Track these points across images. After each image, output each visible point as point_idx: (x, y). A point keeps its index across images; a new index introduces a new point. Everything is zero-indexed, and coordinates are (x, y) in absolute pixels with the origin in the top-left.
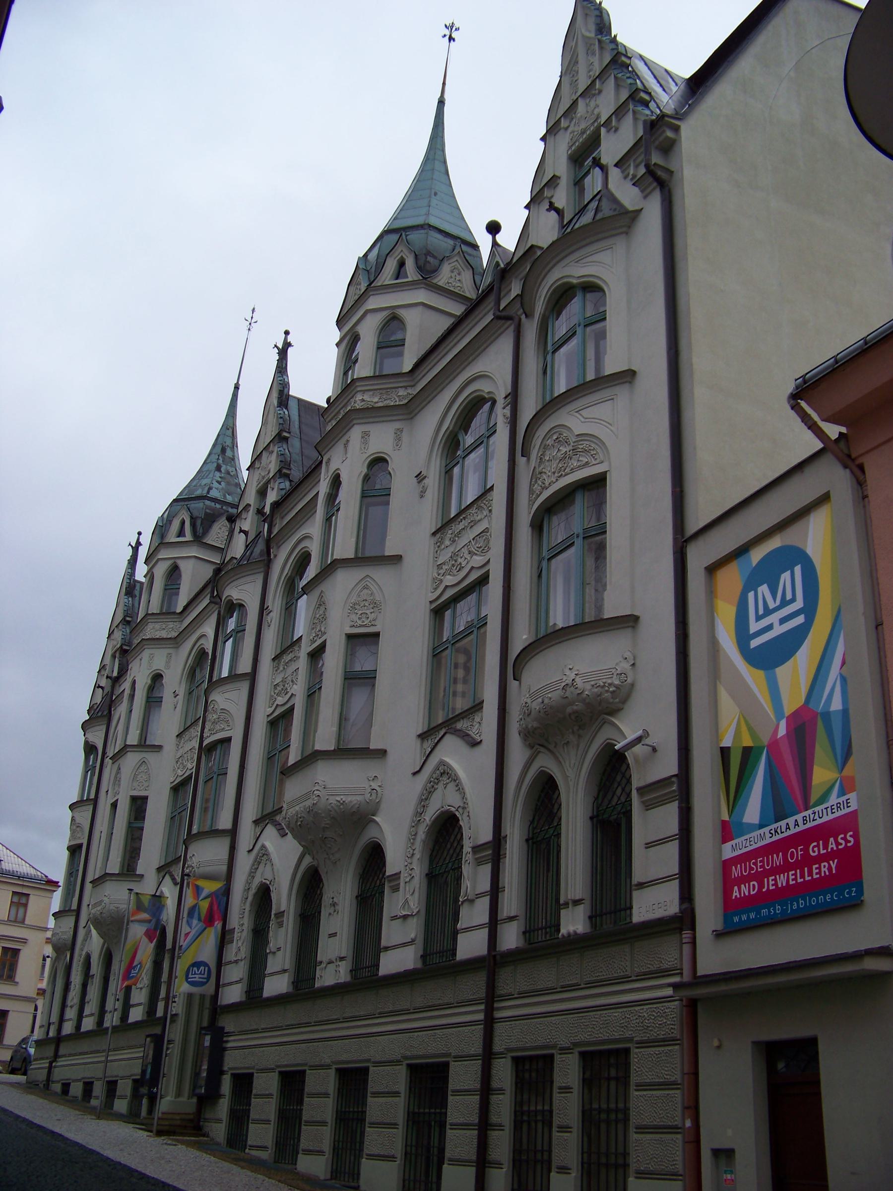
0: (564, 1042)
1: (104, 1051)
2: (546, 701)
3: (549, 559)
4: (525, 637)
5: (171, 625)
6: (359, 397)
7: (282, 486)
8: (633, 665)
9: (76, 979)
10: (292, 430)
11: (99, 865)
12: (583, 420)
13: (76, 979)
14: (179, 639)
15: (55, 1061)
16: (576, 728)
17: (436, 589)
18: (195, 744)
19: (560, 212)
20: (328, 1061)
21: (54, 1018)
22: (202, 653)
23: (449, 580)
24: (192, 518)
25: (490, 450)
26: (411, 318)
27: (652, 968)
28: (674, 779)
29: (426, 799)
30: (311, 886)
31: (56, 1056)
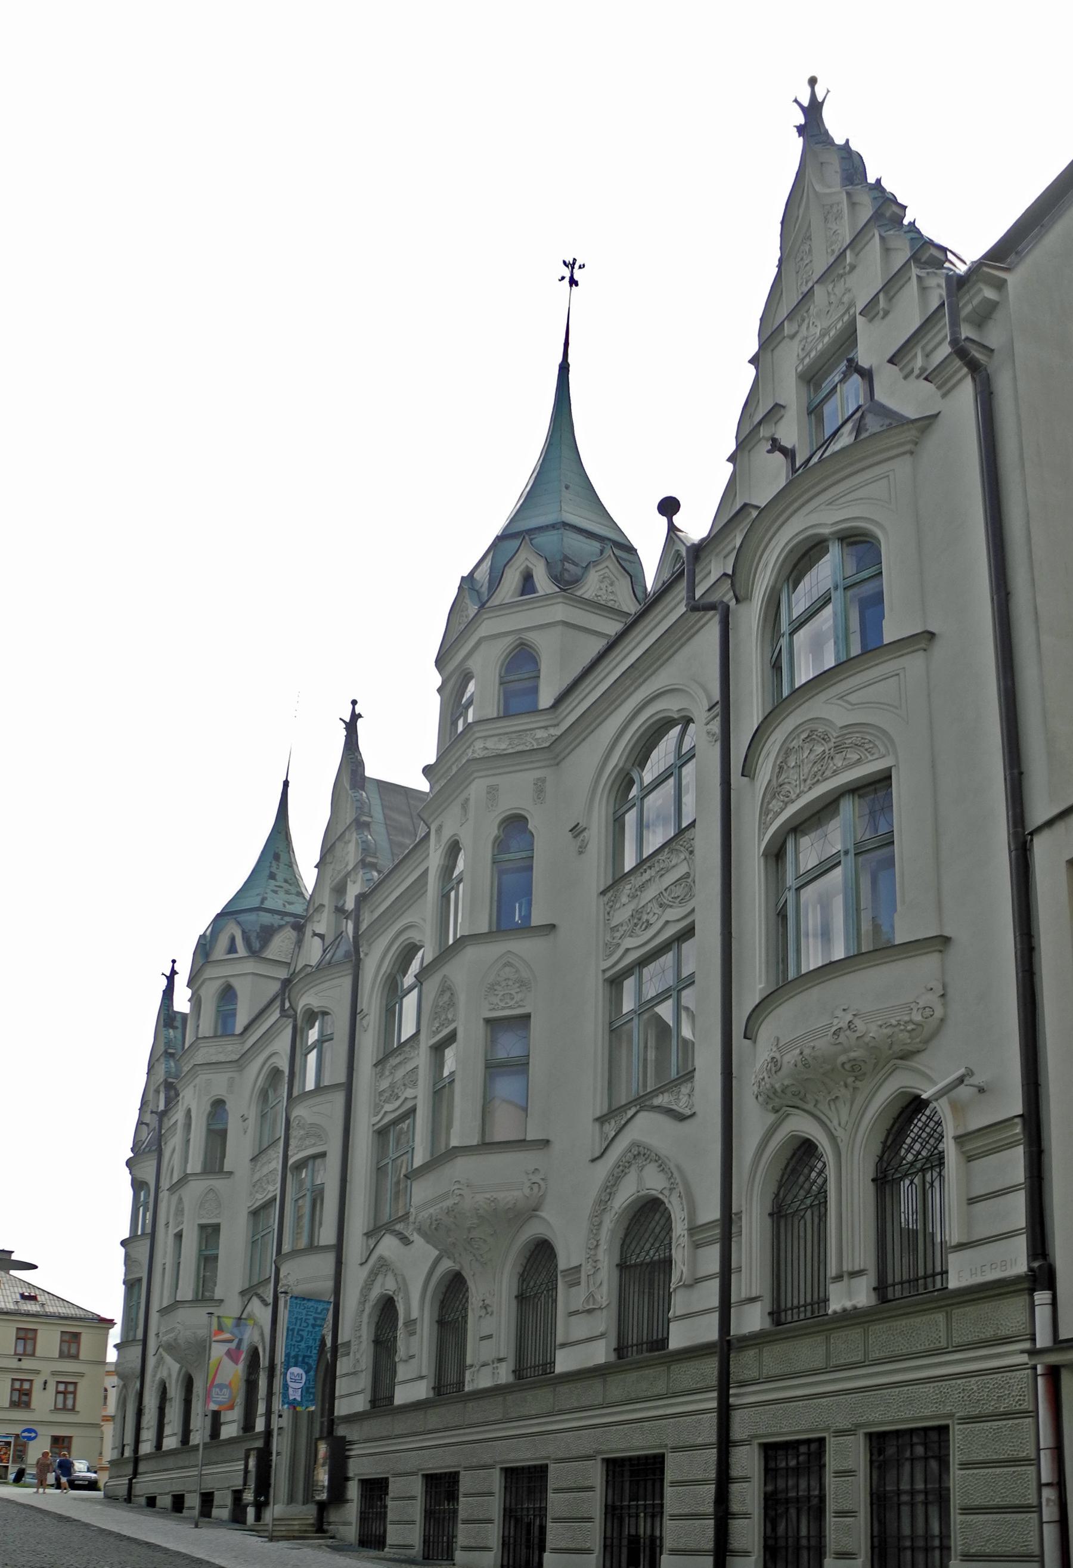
0: (843, 1424)
1: (196, 1466)
2: (806, 1052)
3: (798, 889)
5: (230, 1048)
6: (479, 744)
7: (368, 876)
8: (943, 995)
9: (151, 1402)
10: (373, 813)
11: (166, 1293)
12: (850, 707)
13: (151, 1402)
14: (241, 1062)
15: (134, 1477)
16: (850, 1080)
17: (610, 955)
18: (277, 1164)
19: (789, 454)
20: (490, 1461)
21: (129, 1438)
22: (275, 1073)
23: (388, 1107)
24: (244, 932)
26: (546, 645)
27: (983, 1336)
28: (1017, 1120)
29: (613, 1186)
30: (452, 1293)
31: (135, 1473)
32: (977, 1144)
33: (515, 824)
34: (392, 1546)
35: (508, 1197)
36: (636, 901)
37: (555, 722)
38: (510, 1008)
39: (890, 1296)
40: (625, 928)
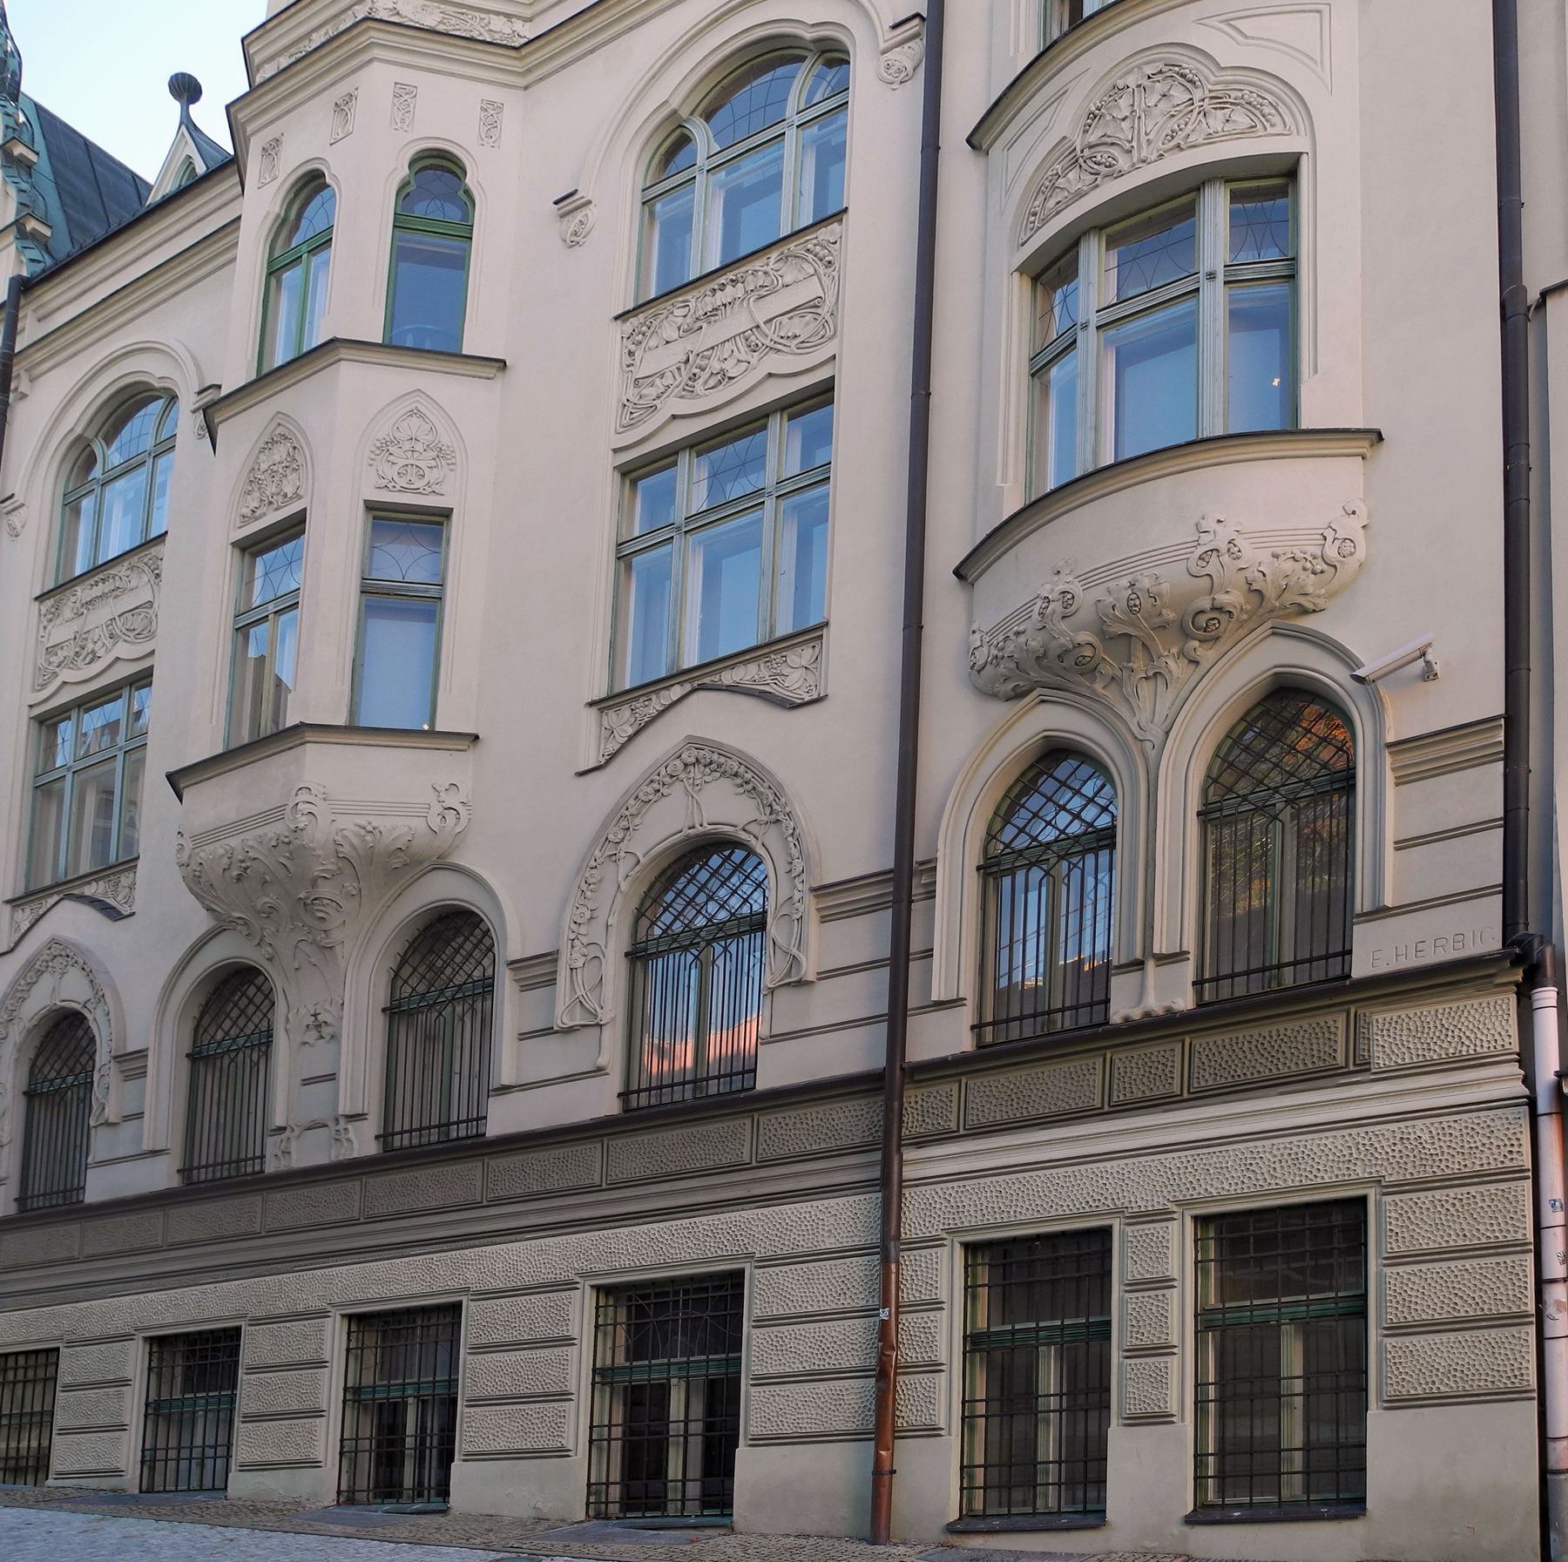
4: (1276, 382)
14: (524, 51)
17: (43, 686)
20: (316, 1304)
25: (159, 479)
32: (1427, 754)
33: (438, 170)
34: (62, 1475)
35: (398, 828)
36: (82, 619)
37: (527, 13)
38: (416, 491)
39: (195, 1179)
40: (668, 380)
